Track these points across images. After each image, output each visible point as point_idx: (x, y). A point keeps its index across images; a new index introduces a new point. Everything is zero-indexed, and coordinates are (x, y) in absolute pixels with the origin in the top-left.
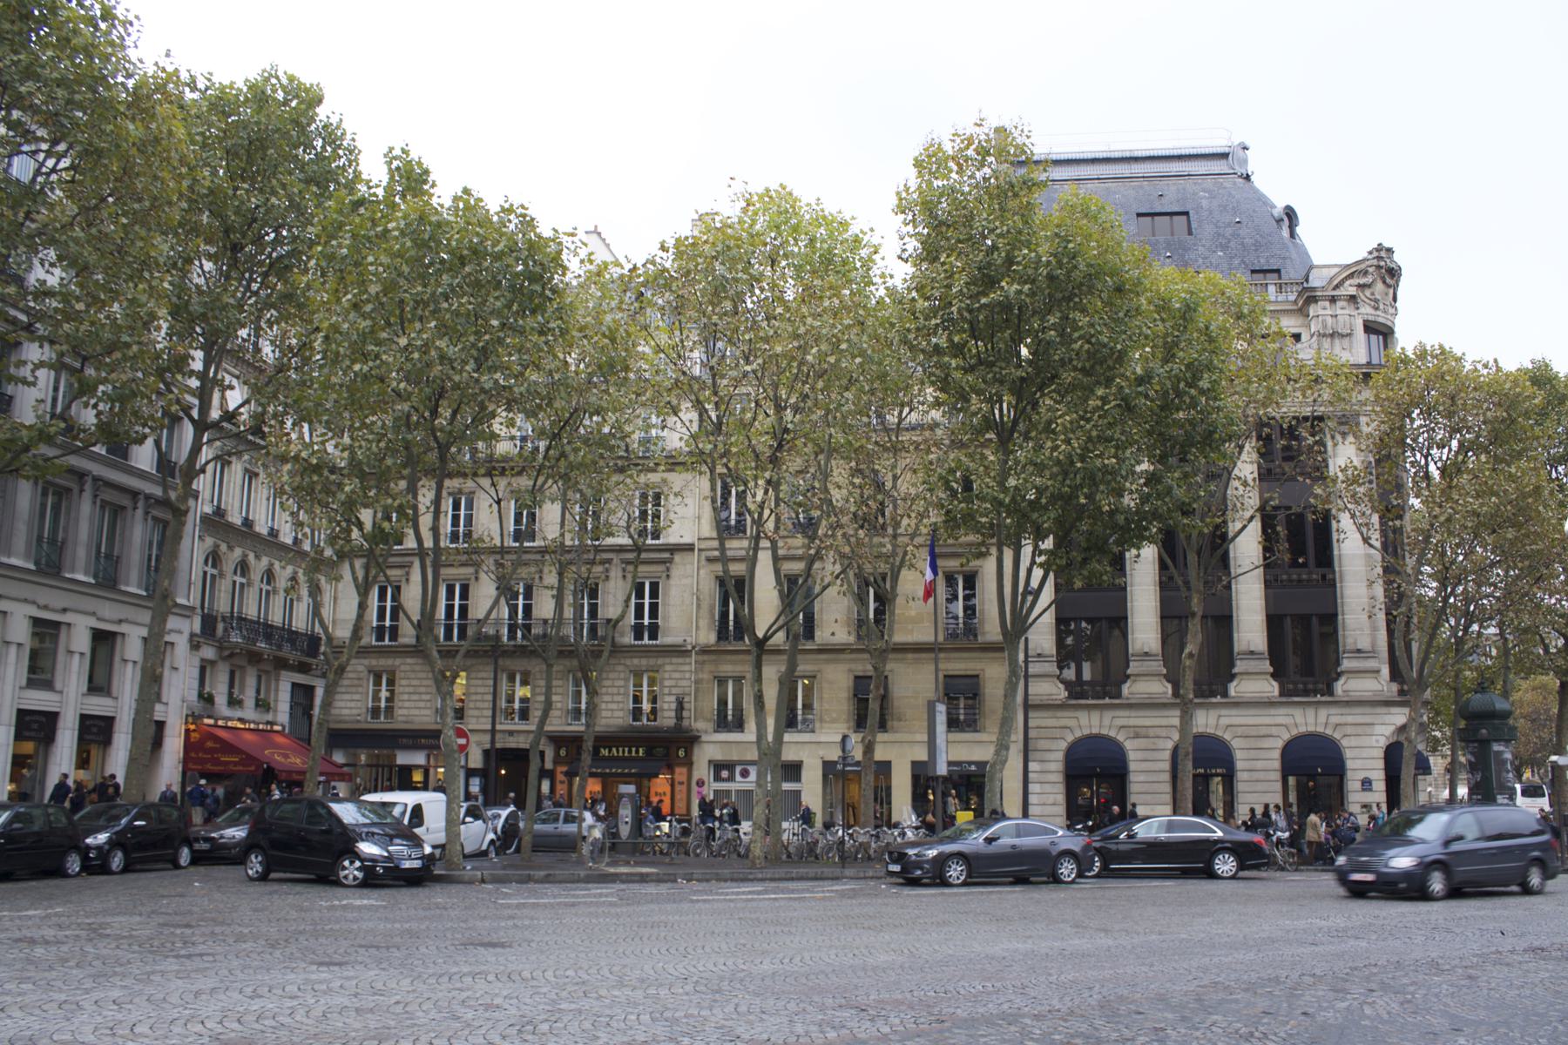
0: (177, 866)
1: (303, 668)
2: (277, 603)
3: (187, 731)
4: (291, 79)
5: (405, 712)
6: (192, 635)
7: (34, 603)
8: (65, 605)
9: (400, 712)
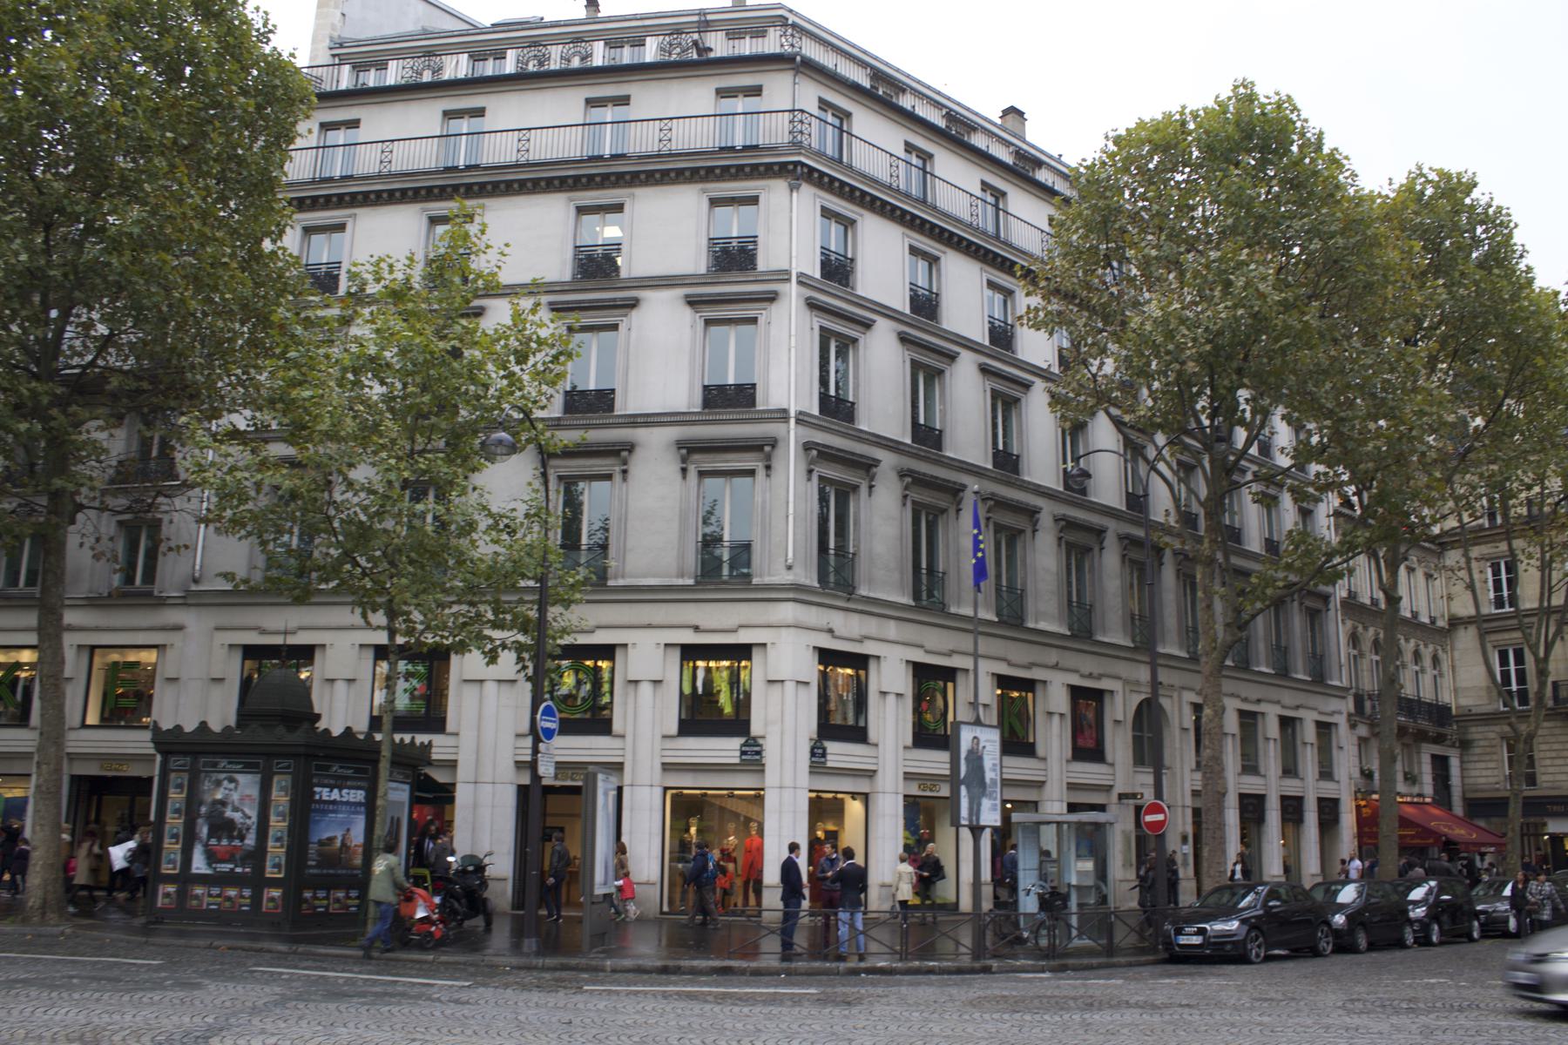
0: (1471, 940)
1: (1439, 739)
2: (1427, 680)
3: (1358, 807)
4: (1441, 173)
5: (1550, 778)
6: (1350, 715)
7: (1076, 671)
8: (1260, 696)
9: (1544, 778)
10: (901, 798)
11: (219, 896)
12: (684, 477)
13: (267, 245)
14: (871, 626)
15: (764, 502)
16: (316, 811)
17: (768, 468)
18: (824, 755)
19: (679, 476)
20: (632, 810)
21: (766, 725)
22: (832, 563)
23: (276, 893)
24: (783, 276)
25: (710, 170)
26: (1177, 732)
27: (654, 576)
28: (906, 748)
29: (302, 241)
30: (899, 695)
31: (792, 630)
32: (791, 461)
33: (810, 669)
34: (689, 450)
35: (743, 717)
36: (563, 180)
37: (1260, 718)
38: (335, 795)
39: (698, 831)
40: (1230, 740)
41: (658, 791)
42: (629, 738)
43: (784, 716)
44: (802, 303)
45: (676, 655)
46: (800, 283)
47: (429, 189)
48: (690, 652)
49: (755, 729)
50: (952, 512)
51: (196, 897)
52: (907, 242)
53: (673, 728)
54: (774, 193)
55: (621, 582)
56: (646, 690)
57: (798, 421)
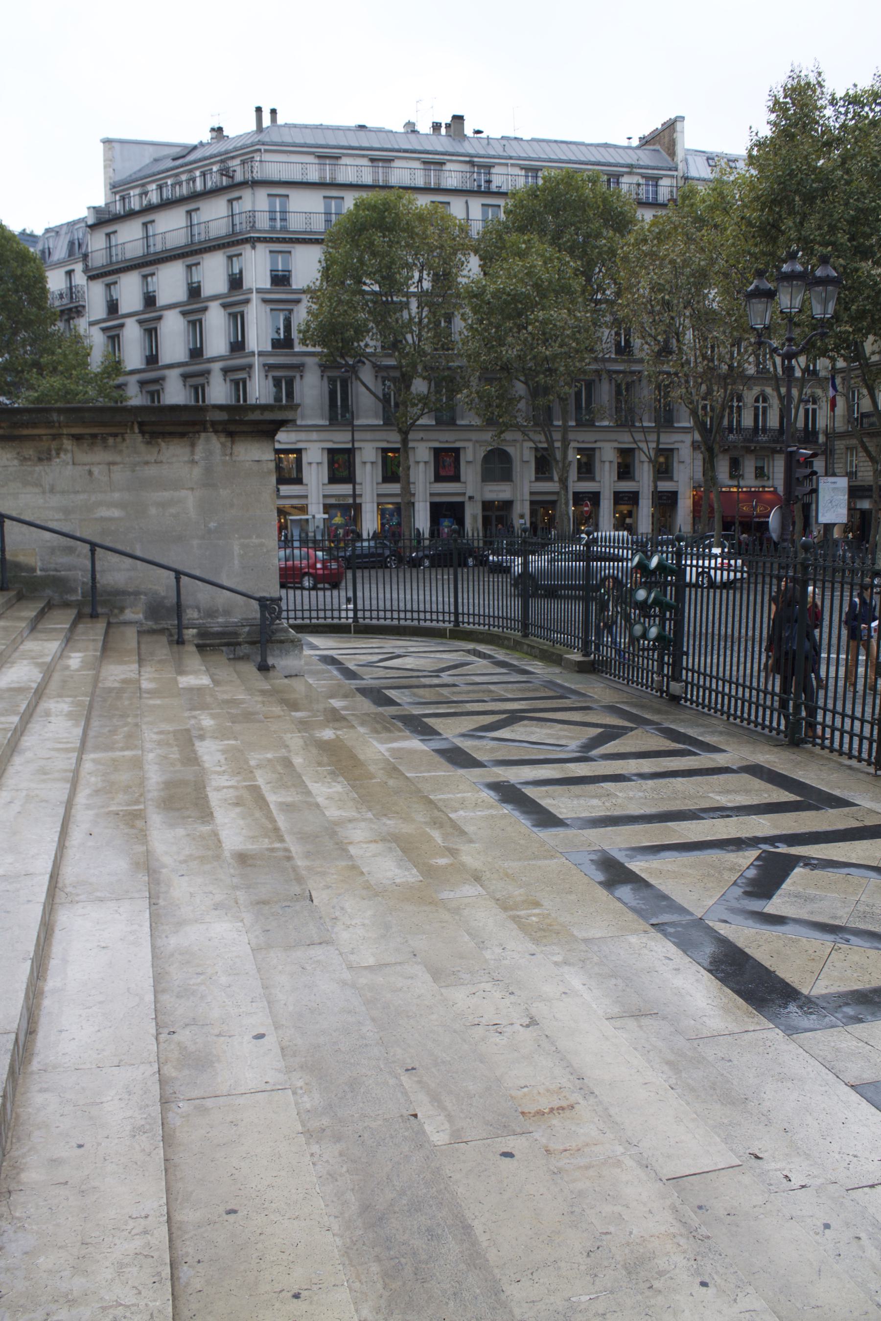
10: (428, 504)
13: (356, 344)
14: (303, 436)
26: (111, 459)
30: (426, 463)
37: (675, 452)
40: (607, 465)
44: (259, 301)
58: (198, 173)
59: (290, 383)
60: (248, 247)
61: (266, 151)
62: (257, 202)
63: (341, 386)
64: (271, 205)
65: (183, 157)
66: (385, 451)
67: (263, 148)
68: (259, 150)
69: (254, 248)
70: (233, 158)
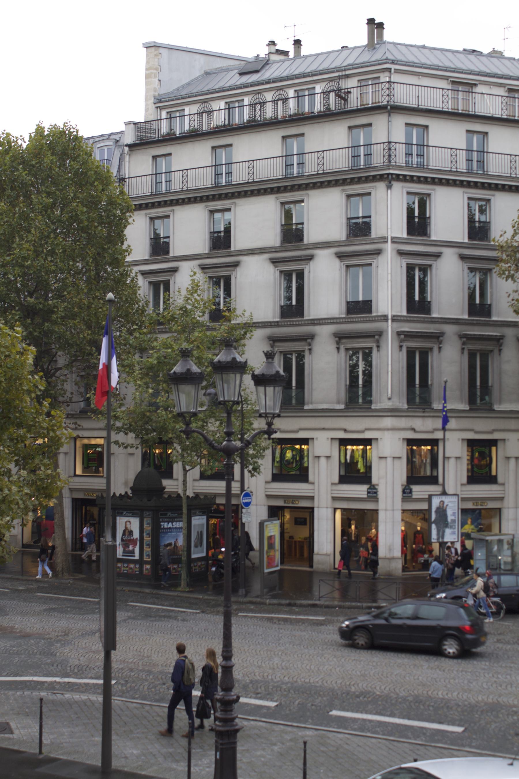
11: (127, 567)
12: (338, 351)
15: (377, 364)
16: (163, 532)
17: (378, 347)
18: (411, 492)
19: (336, 351)
20: (318, 519)
21: (379, 479)
22: (417, 392)
23: (148, 567)
24: (384, 240)
25: (344, 180)
27: (327, 403)
28: (462, 485)
29: (150, 225)
31: (390, 432)
32: (390, 342)
33: (402, 450)
34: (340, 338)
35: (368, 475)
36: (272, 189)
38: (170, 525)
39: (356, 527)
41: (330, 511)
42: (316, 484)
43: (389, 473)
44: (395, 252)
45: (336, 444)
46: (393, 242)
47: (208, 196)
48: (343, 442)
49: (374, 481)
50: (496, 351)
51: (119, 567)
52: (466, 197)
53: (336, 479)
54: (379, 190)
55: (310, 407)
56: (323, 460)
57: (393, 320)
58: (291, 93)
59: (425, 354)
60: (381, 186)
61: (397, 71)
62: (388, 131)
63: (481, 361)
64: (409, 135)
65: (257, 71)
66: (410, 442)
67: (393, 67)
68: (389, 70)
69: (389, 187)
70: (347, 76)
